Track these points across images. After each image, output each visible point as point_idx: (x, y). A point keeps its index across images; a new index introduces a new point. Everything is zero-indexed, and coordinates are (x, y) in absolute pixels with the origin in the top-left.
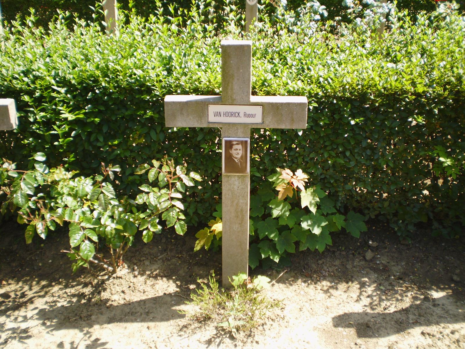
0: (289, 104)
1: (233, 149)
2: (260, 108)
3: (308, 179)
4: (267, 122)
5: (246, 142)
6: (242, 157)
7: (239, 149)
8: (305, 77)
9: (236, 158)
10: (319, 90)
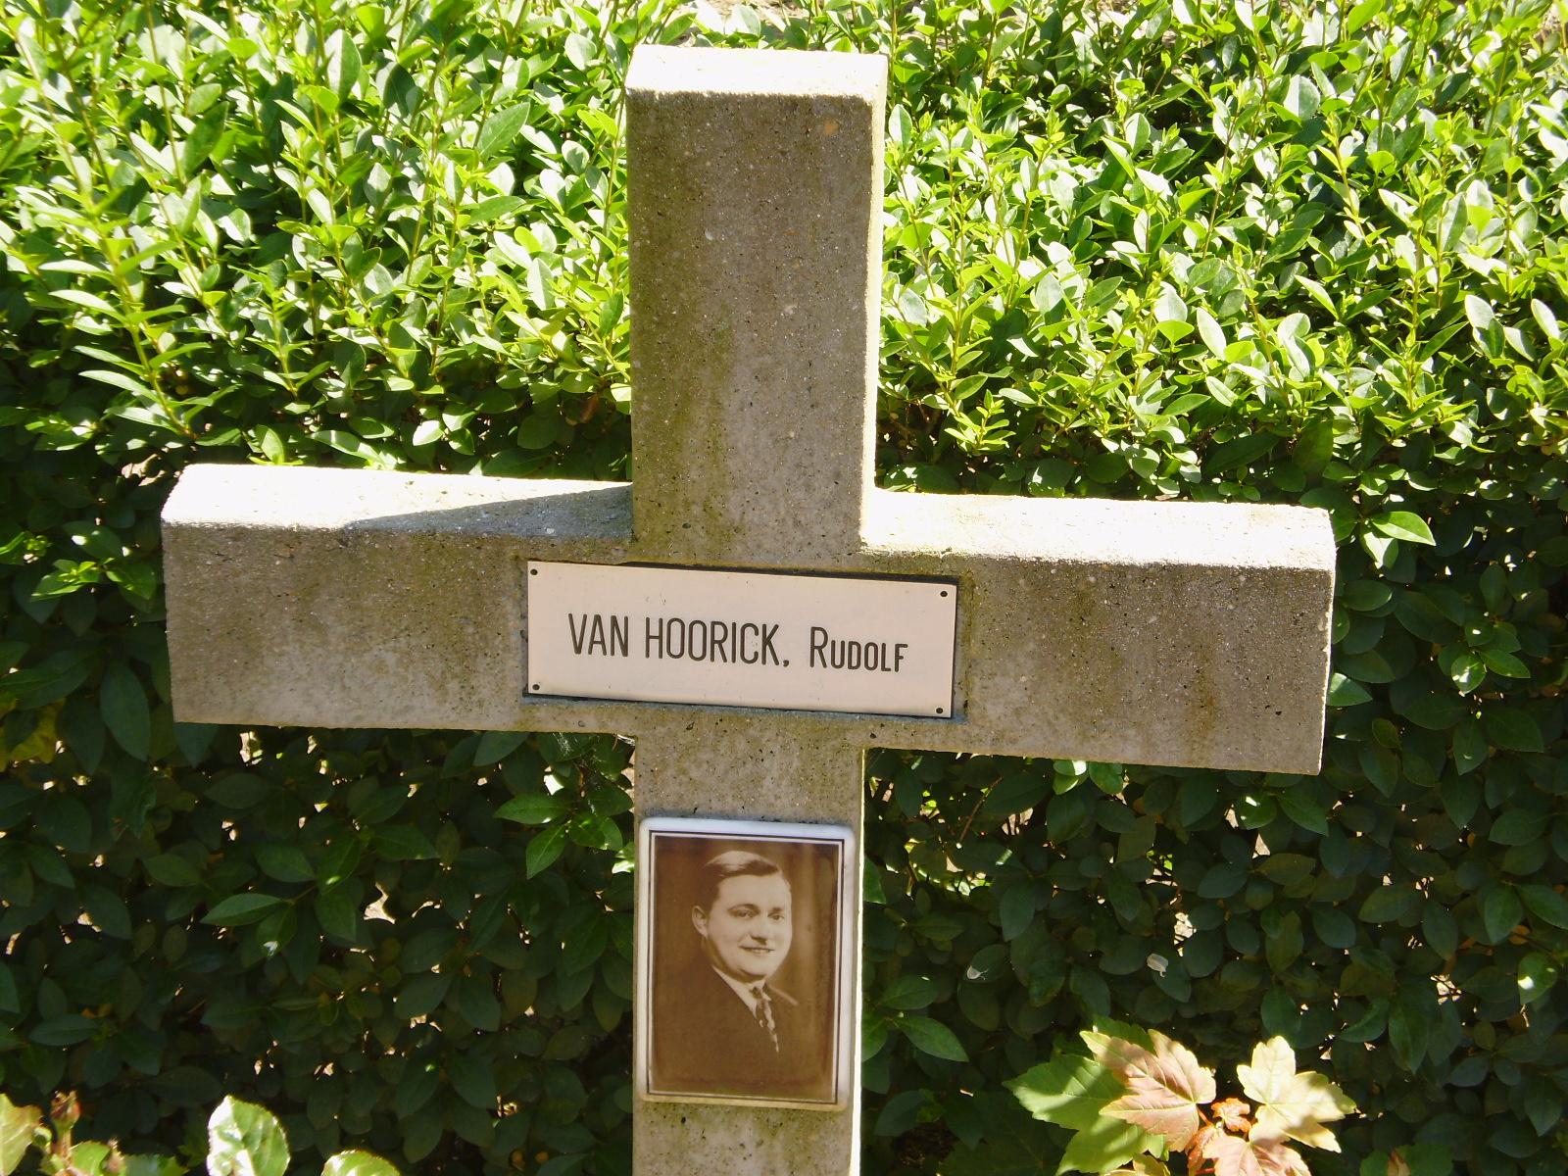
0: (1173, 577)
1: (719, 910)
2: (937, 605)
3: (1340, 1128)
4: (993, 710)
5: (827, 853)
6: (790, 965)
7: (765, 905)
8: (1347, 281)
9: (748, 977)
10: (1446, 409)
